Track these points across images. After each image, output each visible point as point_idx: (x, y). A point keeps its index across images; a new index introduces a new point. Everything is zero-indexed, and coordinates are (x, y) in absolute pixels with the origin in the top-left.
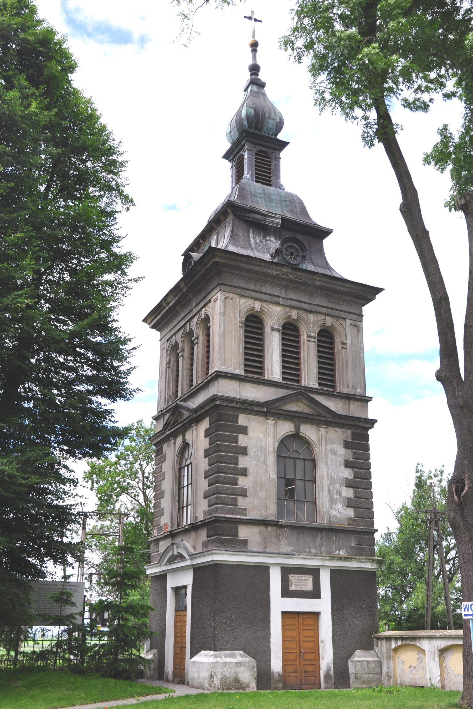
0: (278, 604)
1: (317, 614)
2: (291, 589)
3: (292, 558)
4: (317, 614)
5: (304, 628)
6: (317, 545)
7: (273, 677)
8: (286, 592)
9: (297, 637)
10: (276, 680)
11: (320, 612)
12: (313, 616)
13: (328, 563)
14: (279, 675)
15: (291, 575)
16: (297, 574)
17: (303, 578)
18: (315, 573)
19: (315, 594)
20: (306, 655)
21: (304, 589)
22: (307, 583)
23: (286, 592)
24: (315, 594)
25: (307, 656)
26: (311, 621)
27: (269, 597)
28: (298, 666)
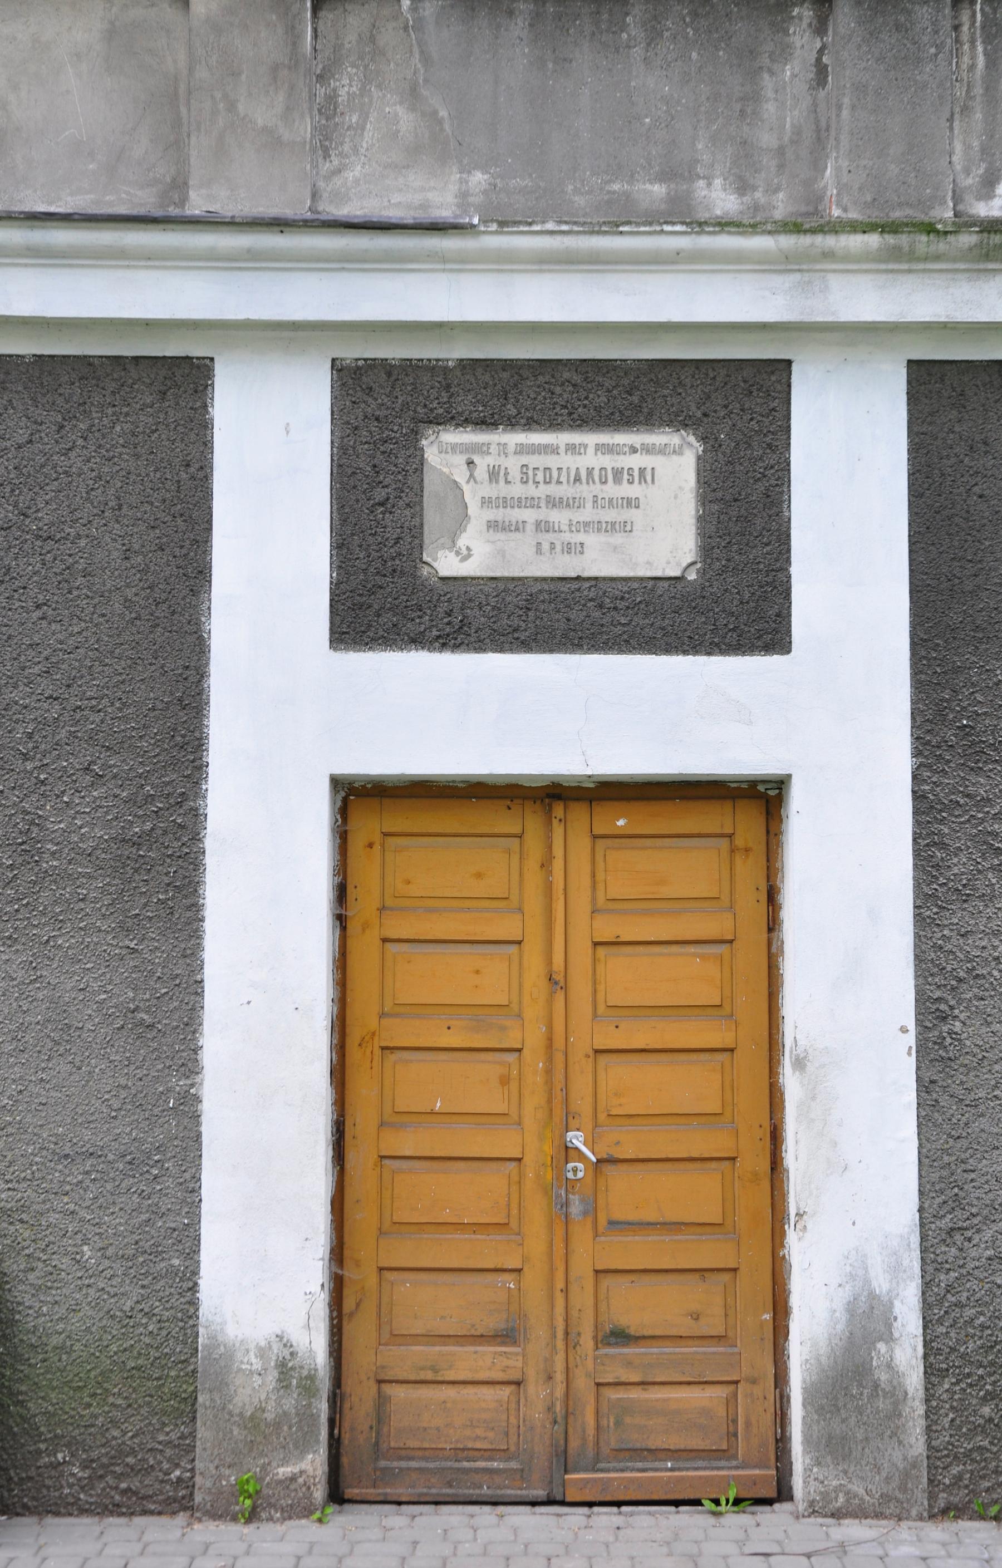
0: (291, 710)
1: (764, 799)
2: (447, 564)
3: (443, 261)
4: (764, 799)
5: (607, 929)
6: (767, 139)
7: (221, 1385)
8: (384, 596)
9: (533, 1011)
10: (254, 1422)
11: (789, 776)
12: (712, 818)
13: (863, 298)
14: (287, 1369)
15: (451, 436)
16: (512, 424)
17: (591, 460)
18: (732, 406)
19: (736, 600)
20: (618, 1179)
21: (599, 560)
22: (643, 505)
23: (384, 596)
24: (736, 600)
25: (627, 1194)
26: (687, 867)
27: (200, 647)
28: (534, 1280)
